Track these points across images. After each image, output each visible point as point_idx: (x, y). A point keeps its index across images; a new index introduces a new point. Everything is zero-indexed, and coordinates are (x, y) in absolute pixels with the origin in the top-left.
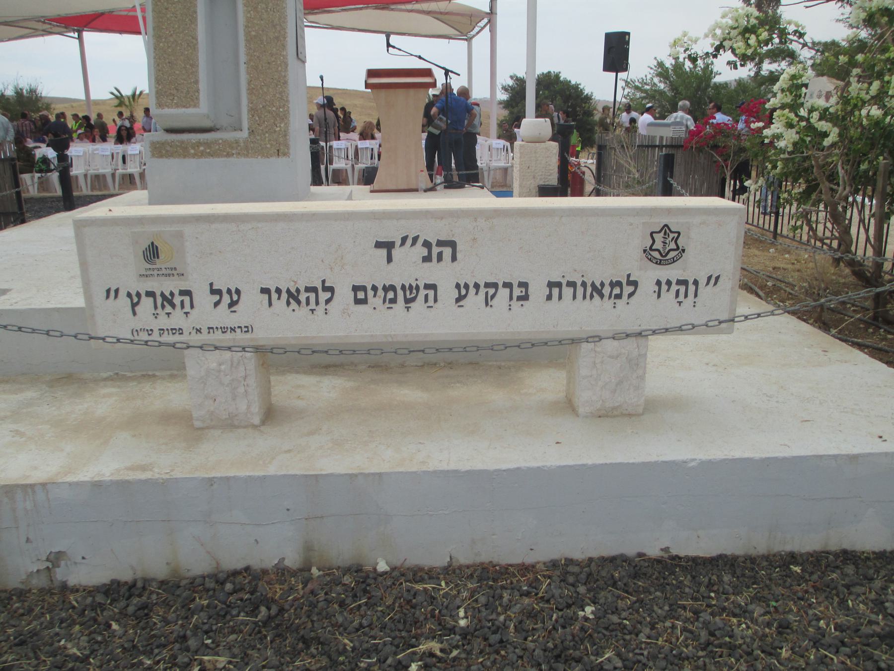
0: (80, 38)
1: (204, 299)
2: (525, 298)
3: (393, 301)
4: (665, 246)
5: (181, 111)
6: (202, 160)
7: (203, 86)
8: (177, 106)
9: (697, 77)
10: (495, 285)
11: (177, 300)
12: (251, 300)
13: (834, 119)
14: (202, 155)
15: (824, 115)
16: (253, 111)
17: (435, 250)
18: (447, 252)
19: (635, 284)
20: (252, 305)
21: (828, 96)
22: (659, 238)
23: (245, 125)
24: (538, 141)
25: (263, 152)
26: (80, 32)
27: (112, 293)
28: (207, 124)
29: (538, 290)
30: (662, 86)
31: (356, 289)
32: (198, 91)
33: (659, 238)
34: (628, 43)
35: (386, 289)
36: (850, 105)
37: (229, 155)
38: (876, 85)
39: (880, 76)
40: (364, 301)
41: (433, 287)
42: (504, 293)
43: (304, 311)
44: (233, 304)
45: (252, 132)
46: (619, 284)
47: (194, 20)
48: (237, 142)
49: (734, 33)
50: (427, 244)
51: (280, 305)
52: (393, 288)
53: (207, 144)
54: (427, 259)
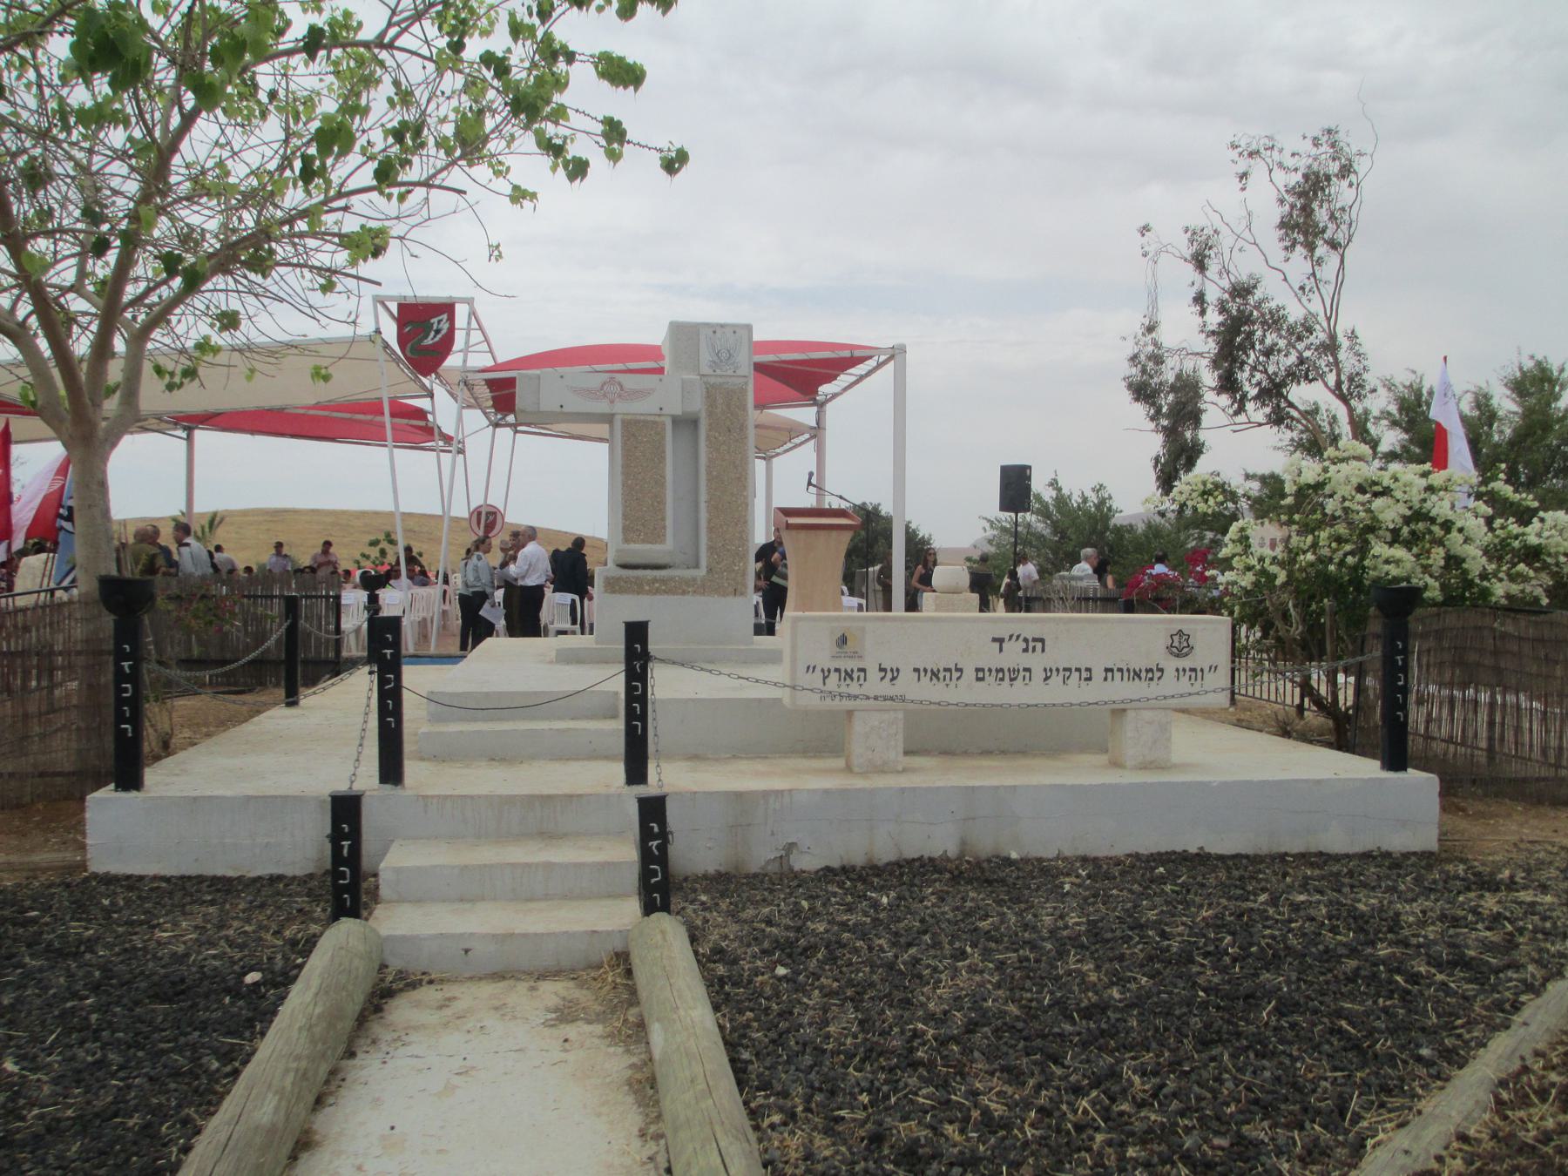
0: (190, 439)
1: (874, 674)
2: (1089, 679)
3: (1002, 679)
4: (1180, 646)
5: (648, 546)
6: (658, 597)
7: (669, 522)
8: (643, 541)
9: (1087, 513)
10: (1069, 670)
11: (855, 675)
12: (907, 676)
13: (1282, 564)
14: (657, 592)
15: (1274, 560)
16: (711, 549)
17: (1031, 644)
18: (1039, 645)
19: (1161, 670)
20: (906, 680)
21: (1273, 546)
22: (1176, 638)
23: (704, 562)
24: (956, 591)
25: (720, 591)
26: (189, 430)
27: (811, 669)
28: (661, 561)
29: (1098, 674)
30: (1040, 526)
31: (977, 670)
32: (664, 527)
33: (1176, 638)
34: (1029, 478)
35: (998, 671)
36: (1293, 554)
37: (684, 593)
38: (1310, 538)
39: (1312, 532)
40: (982, 679)
41: (1028, 670)
42: (1075, 675)
43: (942, 684)
44: (893, 679)
45: (710, 570)
46: (1151, 670)
47: (662, 458)
48: (694, 579)
49: (1195, 495)
50: (1026, 640)
51: (925, 680)
52: (1002, 670)
53: (663, 581)
54: (1025, 650)
